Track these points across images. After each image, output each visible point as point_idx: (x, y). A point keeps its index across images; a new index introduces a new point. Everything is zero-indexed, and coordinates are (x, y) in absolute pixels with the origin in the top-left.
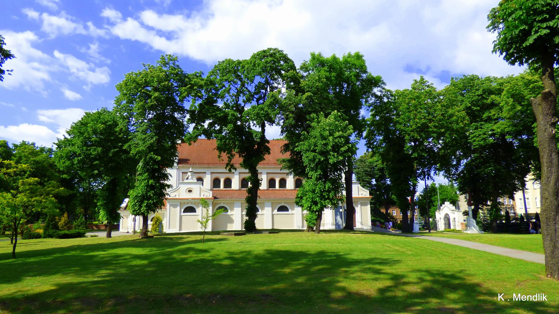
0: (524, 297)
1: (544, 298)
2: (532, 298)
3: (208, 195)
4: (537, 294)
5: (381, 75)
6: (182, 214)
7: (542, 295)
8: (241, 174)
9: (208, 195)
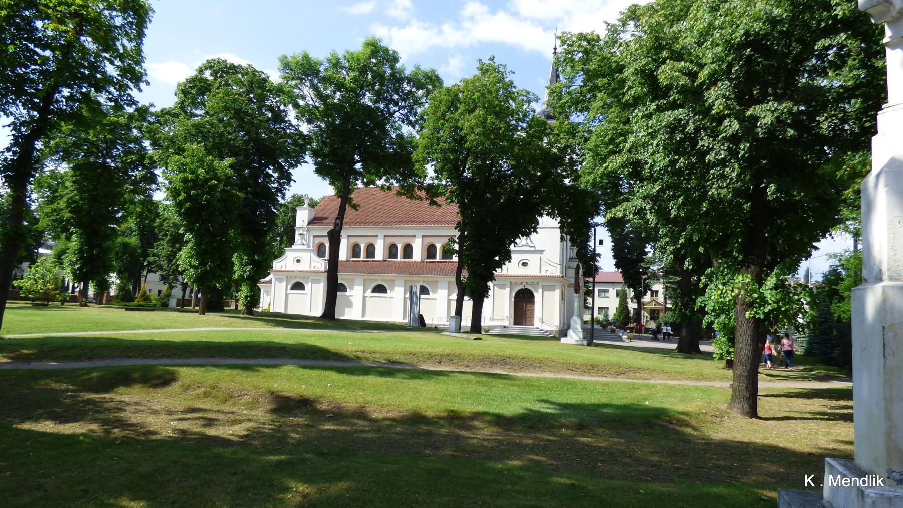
0: (846, 480)
1: (878, 482)
2: (859, 482)
3: (319, 268)
4: (867, 476)
5: (435, 68)
6: (289, 291)
8: (386, 238)
9: (319, 268)
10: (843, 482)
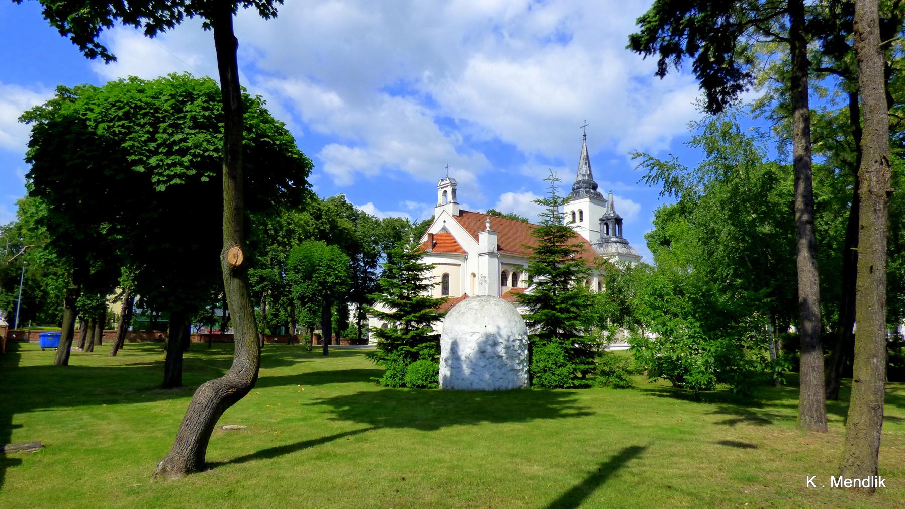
1: (880, 483)
4: (869, 477)
7: (878, 478)
10: (845, 483)
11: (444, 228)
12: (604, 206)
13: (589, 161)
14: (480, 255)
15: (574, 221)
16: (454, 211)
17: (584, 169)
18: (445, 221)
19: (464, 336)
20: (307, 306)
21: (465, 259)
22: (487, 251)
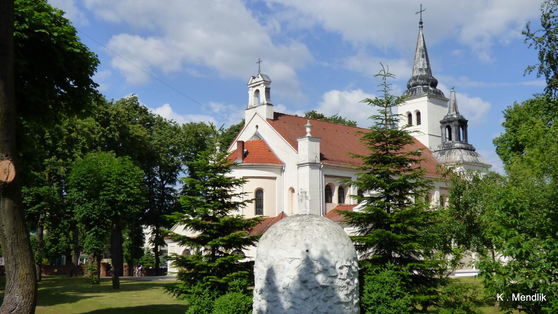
0: (523, 297)
10: (521, 298)
11: (256, 135)
12: (446, 106)
13: (426, 52)
14: (300, 165)
15: (410, 124)
16: (268, 114)
17: (421, 63)
18: (257, 127)
19: (281, 263)
20: (93, 229)
21: (282, 171)
22: (307, 161)
